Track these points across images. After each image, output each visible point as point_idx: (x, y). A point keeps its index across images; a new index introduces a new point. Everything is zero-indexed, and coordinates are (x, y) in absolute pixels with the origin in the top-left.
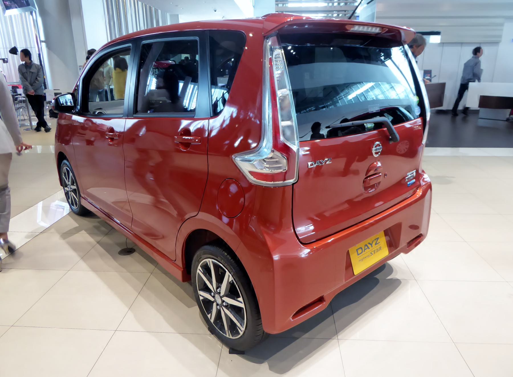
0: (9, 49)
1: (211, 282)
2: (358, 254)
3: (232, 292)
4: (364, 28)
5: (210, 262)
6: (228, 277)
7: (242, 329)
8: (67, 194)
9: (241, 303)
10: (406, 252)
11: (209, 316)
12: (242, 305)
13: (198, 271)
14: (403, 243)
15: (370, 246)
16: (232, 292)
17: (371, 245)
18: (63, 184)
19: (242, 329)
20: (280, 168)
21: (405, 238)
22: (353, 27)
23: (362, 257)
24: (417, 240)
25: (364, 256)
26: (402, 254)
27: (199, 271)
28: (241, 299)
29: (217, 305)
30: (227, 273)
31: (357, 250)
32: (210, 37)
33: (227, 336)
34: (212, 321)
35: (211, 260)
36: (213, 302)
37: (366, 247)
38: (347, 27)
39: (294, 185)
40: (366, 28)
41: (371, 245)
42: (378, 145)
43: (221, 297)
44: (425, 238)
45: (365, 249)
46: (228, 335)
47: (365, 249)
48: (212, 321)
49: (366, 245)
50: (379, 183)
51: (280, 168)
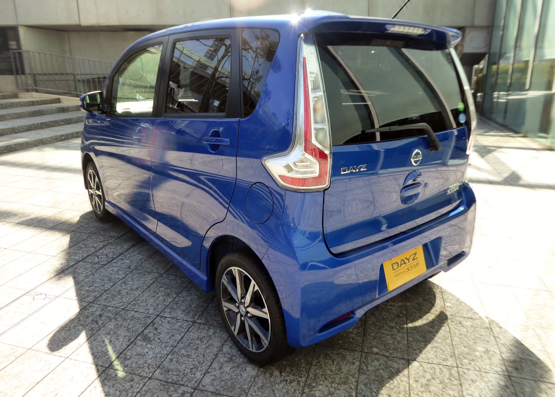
0: (47, 350)
1: (249, 325)
2: (393, 270)
3: (257, 302)
4: (413, 30)
5: (235, 270)
6: (254, 286)
7: (266, 342)
8: (91, 196)
9: (266, 313)
10: (446, 271)
11: (233, 328)
12: (268, 317)
13: (223, 280)
14: (443, 262)
15: (406, 261)
16: (257, 302)
17: (408, 260)
18: (87, 186)
19: (266, 342)
20: (312, 172)
21: (445, 253)
22: (393, 27)
23: (397, 273)
24: (458, 257)
25: (400, 272)
26: (442, 273)
27: (225, 280)
28: (266, 310)
29: (241, 316)
30: (253, 282)
31: (392, 265)
32: (440, 238)
33: (251, 349)
34: (236, 333)
35: (236, 268)
36: (237, 313)
37: (403, 262)
38: (387, 27)
39: (326, 192)
40: (412, 29)
41: (408, 260)
42: (418, 154)
43: (246, 308)
44: (467, 257)
45: (401, 264)
46: (252, 348)
47: (401, 264)
48: (236, 333)
49: (403, 260)
50: (418, 194)
51: (312, 172)
